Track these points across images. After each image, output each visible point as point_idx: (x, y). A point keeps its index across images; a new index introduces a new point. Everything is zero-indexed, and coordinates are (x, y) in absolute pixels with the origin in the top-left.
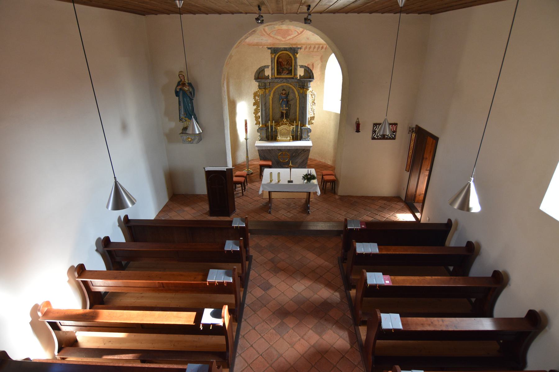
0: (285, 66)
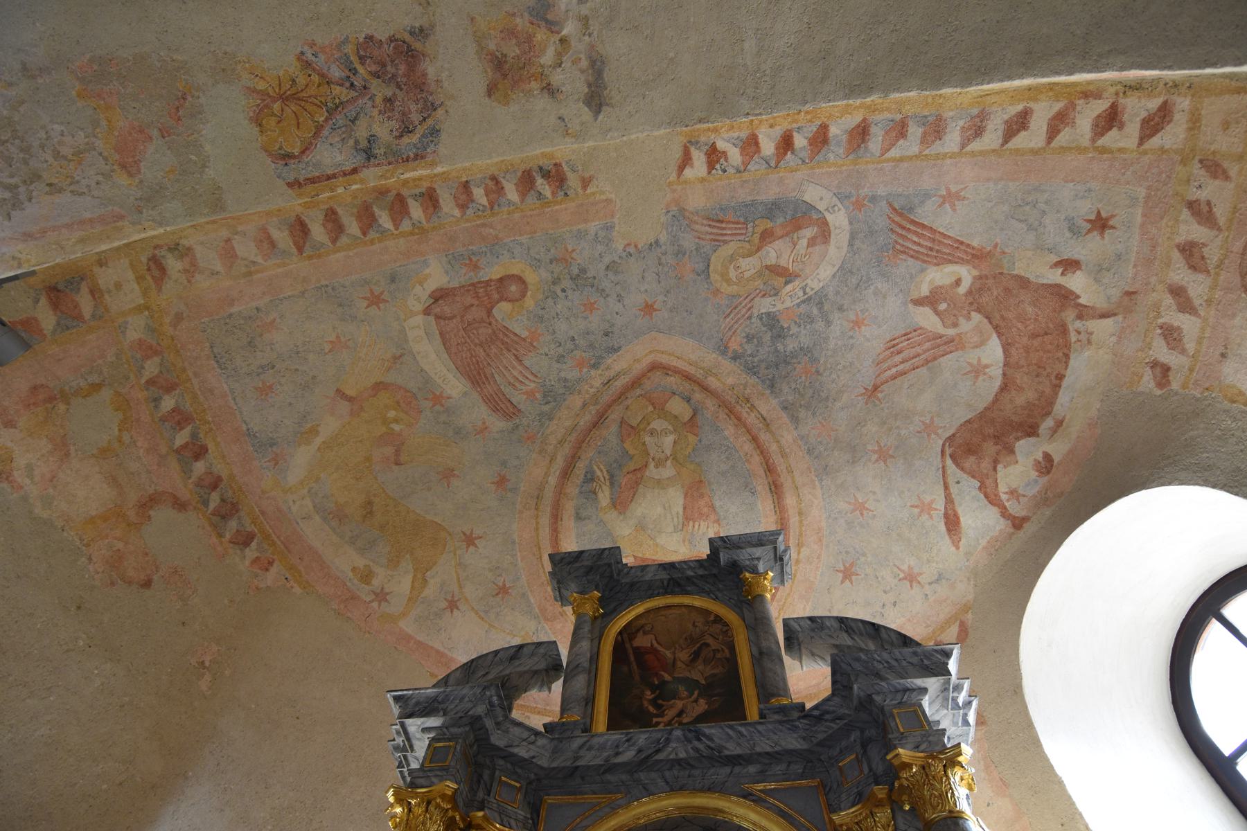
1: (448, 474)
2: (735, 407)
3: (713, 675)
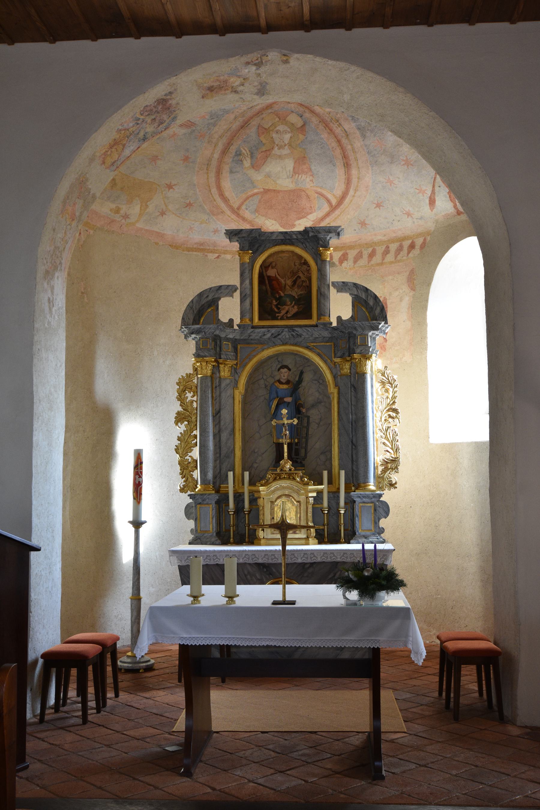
0: (289, 292)
1: (155, 159)
2: (329, 124)
3: (301, 294)
